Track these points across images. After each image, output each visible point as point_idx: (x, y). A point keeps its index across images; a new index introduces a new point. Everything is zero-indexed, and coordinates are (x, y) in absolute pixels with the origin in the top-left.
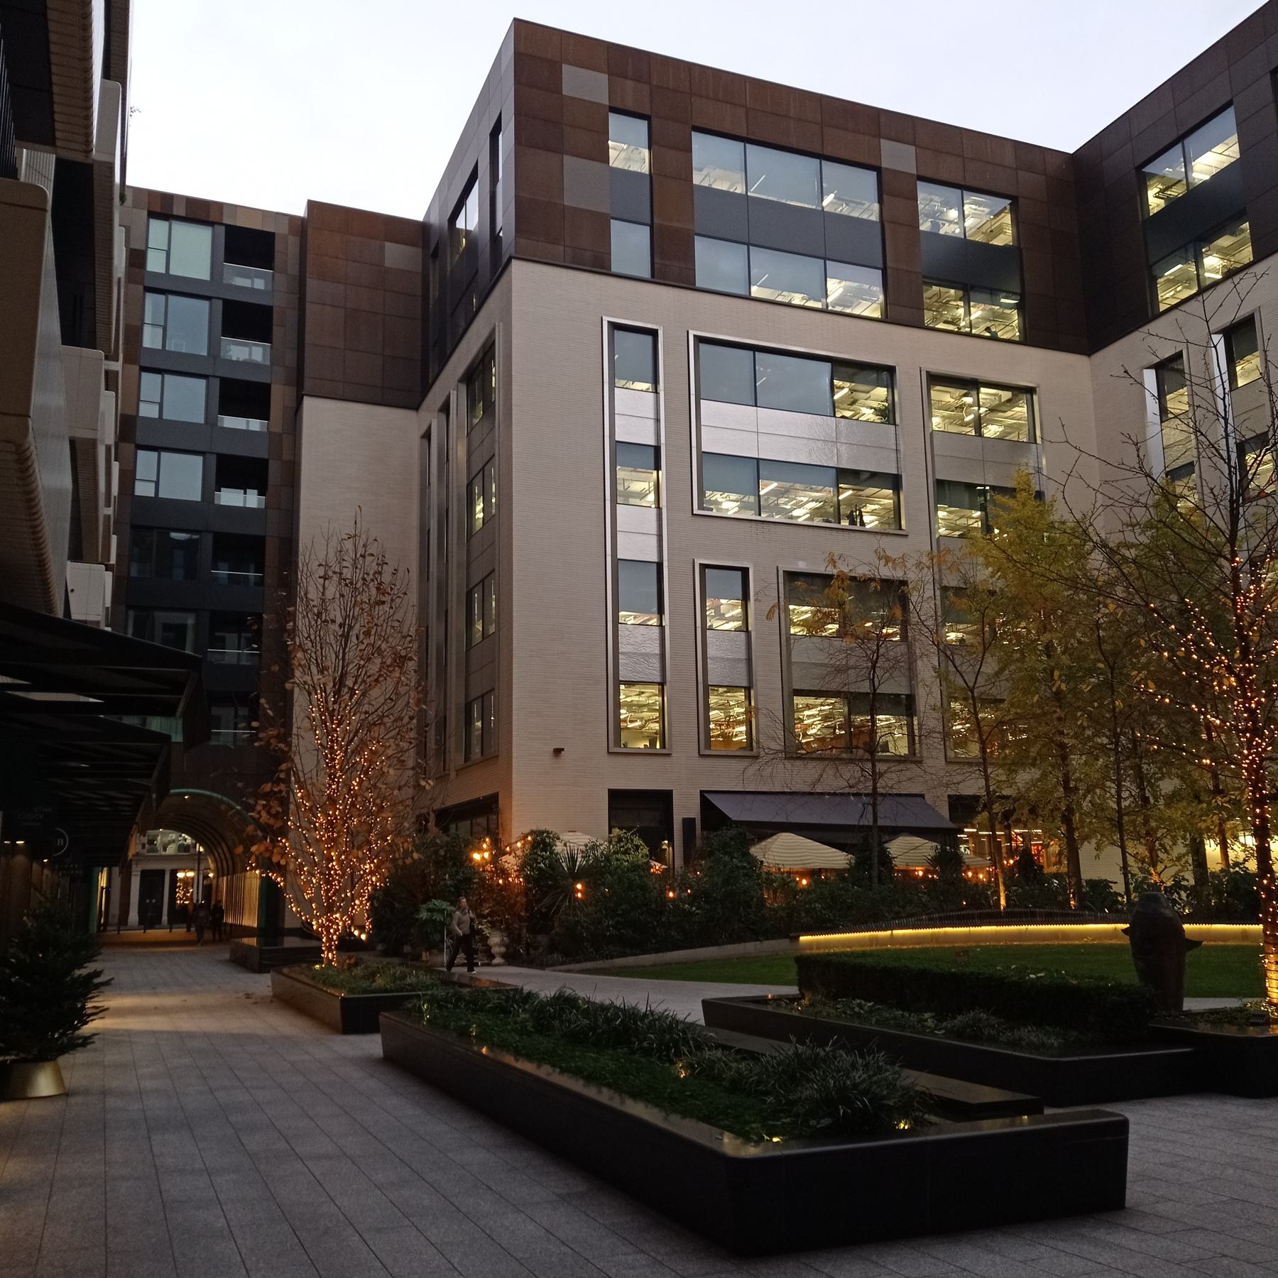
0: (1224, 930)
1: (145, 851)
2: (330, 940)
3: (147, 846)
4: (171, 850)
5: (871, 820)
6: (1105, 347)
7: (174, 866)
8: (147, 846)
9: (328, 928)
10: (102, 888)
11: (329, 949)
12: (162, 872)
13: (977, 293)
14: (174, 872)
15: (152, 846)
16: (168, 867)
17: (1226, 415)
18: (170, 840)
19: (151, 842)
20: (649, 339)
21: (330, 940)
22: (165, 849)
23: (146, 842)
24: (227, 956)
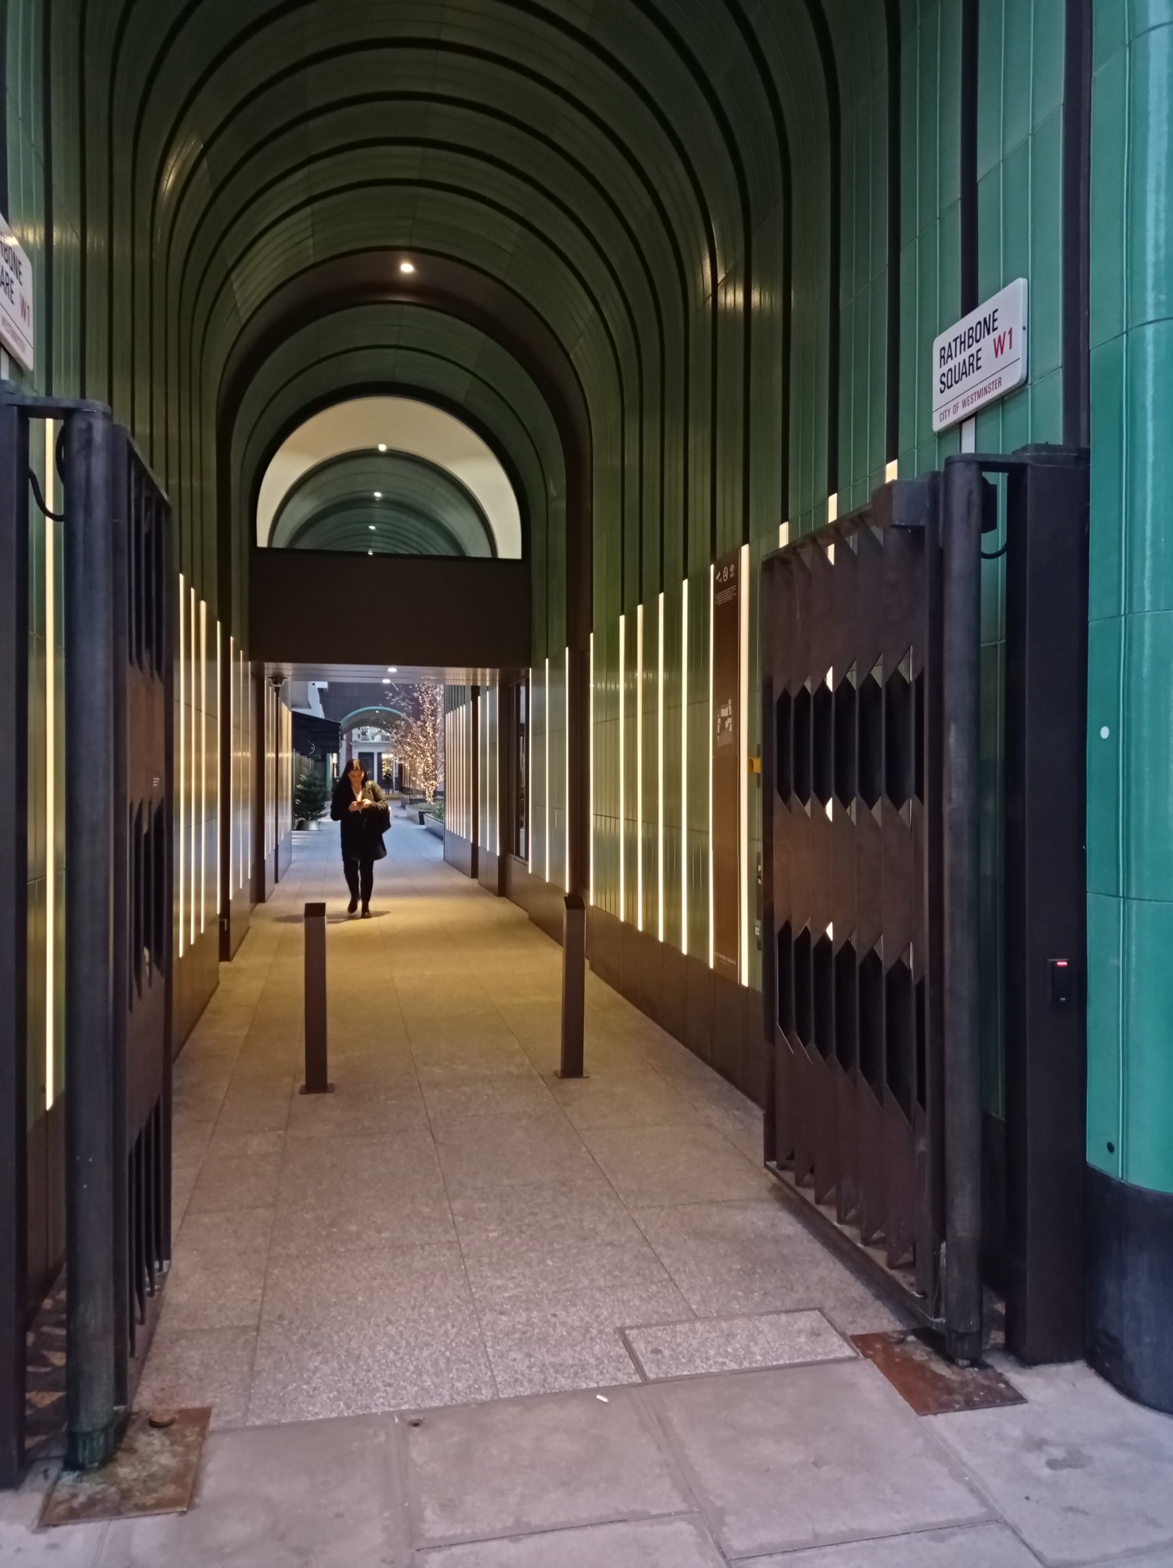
0: (854, 750)
1: (360, 739)
2: (429, 793)
3: (361, 736)
4: (378, 739)
5: (42, 393)
6: (1086, 997)
7: (380, 751)
8: (361, 736)
9: (428, 787)
10: (334, 764)
11: (429, 797)
12: (371, 755)
13: (1108, 1384)
14: (380, 754)
15: (365, 736)
16: (375, 751)
17: (983, 1501)
18: (374, 734)
19: (364, 734)
20: (1114, 893)
21: (429, 793)
22: (373, 739)
23: (360, 733)
24: (400, 805)
